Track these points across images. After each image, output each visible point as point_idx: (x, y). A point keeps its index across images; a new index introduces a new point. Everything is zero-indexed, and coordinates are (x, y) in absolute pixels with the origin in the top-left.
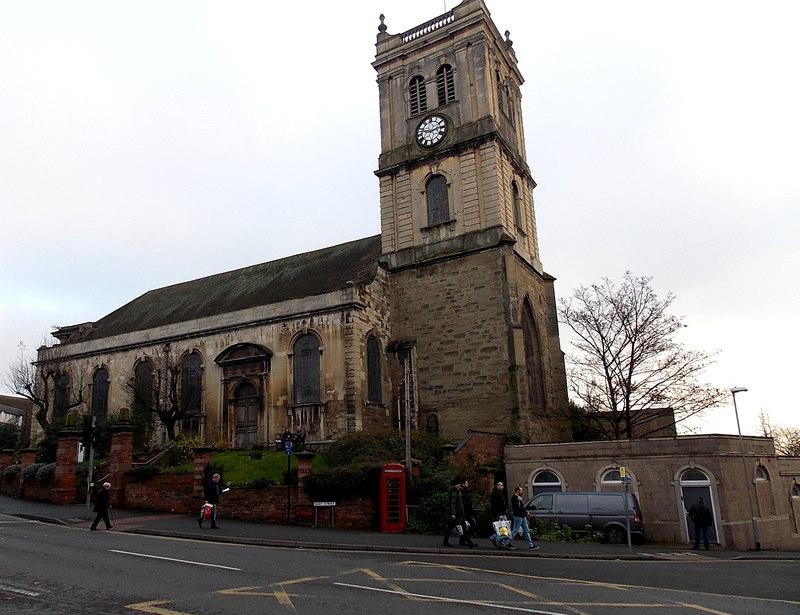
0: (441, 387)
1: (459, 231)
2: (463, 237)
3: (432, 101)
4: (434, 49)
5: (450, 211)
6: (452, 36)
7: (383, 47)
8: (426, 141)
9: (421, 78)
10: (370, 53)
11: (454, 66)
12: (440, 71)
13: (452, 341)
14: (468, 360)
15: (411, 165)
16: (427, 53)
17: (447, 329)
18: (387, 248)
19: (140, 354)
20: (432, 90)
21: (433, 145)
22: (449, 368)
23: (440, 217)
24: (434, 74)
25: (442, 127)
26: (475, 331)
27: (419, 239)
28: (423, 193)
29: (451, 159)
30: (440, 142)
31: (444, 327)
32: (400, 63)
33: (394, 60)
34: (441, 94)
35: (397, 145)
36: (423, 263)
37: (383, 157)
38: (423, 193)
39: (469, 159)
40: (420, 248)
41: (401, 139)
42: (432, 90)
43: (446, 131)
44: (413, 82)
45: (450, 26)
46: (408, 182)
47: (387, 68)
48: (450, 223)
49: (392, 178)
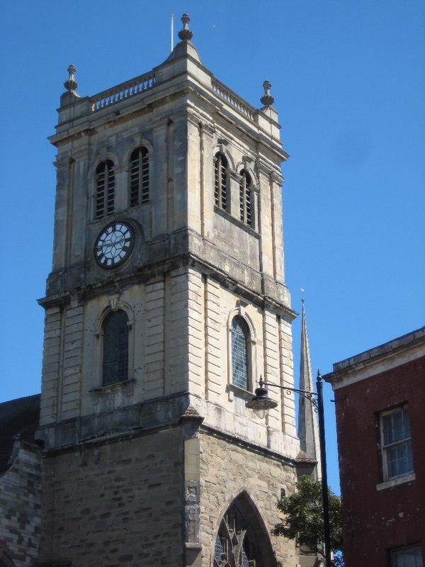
2: (141, 406)
4: (129, 123)
5: (130, 366)
6: (151, 107)
7: (67, 114)
8: (107, 259)
9: (110, 163)
10: (49, 120)
11: (150, 149)
12: (134, 156)
15: (87, 295)
16: (119, 127)
17: (113, 546)
18: (46, 417)
19: (279, 404)
20: (122, 180)
21: (115, 266)
23: (117, 369)
24: (126, 157)
26: (145, 551)
27: (91, 407)
28: (98, 336)
29: (136, 288)
30: (123, 261)
31: (107, 543)
32: (85, 139)
34: (134, 188)
35: (73, 261)
36: (83, 440)
37: (54, 279)
38: (98, 336)
39: (157, 289)
41: (78, 253)
42: (122, 180)
43: (132, 246)
44: (100, 168)
45: (143, 95)
46: (80, 319)
47: (67, 147)
49: (61, 312)
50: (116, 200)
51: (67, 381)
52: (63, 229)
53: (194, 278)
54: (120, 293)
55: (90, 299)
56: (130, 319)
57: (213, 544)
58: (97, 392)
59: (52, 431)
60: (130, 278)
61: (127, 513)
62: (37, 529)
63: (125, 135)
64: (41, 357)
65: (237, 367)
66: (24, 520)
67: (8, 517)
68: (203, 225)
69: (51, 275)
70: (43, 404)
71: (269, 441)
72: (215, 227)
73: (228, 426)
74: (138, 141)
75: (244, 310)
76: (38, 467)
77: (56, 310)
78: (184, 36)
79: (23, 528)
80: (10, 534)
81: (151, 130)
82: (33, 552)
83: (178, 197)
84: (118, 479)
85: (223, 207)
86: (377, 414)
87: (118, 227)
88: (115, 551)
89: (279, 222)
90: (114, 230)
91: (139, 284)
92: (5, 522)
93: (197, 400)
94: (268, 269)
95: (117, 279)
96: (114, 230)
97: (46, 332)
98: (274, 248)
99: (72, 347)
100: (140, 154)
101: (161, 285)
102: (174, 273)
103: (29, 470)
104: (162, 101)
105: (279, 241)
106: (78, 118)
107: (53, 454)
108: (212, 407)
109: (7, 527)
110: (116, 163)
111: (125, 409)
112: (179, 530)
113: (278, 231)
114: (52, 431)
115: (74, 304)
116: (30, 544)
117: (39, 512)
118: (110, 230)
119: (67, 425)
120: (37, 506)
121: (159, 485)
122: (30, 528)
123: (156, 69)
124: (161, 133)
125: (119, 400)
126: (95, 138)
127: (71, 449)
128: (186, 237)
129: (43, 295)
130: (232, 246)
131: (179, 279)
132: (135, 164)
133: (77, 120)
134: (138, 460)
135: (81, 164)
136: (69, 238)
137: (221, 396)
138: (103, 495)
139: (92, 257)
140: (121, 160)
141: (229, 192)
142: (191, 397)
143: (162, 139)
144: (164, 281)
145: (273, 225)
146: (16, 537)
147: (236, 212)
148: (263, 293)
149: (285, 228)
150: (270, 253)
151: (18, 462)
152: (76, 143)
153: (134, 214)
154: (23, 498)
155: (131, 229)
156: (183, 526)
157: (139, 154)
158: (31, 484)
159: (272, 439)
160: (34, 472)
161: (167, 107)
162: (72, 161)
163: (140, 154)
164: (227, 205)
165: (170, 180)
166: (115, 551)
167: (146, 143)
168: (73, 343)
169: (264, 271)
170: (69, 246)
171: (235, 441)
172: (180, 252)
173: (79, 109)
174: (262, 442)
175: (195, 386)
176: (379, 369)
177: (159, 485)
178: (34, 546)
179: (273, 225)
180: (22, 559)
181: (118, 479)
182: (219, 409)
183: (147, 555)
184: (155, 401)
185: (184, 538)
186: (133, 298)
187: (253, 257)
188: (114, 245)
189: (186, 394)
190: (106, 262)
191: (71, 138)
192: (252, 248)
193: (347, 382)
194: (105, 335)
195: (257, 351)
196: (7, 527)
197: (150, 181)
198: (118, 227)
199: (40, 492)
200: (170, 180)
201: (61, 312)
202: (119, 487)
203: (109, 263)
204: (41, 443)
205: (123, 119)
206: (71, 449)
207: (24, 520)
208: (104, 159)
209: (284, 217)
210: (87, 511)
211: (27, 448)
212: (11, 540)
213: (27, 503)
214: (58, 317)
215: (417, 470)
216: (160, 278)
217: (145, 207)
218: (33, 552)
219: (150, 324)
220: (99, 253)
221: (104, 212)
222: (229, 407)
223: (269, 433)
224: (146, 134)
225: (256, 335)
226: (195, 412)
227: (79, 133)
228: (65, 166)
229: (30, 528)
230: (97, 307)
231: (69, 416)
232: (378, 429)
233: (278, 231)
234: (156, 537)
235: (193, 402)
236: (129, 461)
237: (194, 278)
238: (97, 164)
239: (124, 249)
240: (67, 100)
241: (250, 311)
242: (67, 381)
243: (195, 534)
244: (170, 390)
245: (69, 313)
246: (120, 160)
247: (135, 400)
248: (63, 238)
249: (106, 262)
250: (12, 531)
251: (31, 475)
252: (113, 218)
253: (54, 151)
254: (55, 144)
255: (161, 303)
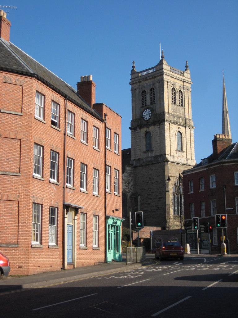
0: (147, 210)
1: (154, 154)
3: (148, 102)
4: (149, 81)
6: (155, 77)
9: (145, 92)
10: (128, 78)
12: (151, 90)
13: (150, 195)
14: (155, 201)
15: (141, 127)
16: (147, 82)
17: (150, 190)
20: (148, 97)
21: (147, 120)
22: (149, 204)
23: (149, 149)
24: (149, 91)
25: (150, 114)
26: (157, 191)
28: (144, 138)
30: (149, 119)
31: (148, 189)
32: (138, 84)
33: (136, 83)
34: (151, 99)
35: (137, 118)
37: (132, 122)
38: (144, 138)
40: (142, 159)
42: (148, 97)
43: (151, 115)
44: (143, 92)
47: (134, 85)
48: (152, 151)
49: (135, 131)
50: (147, 101)
51: (137, 149)
52: (134, 108)
53: (133, 240)
54: (149, 127)
55: (142, 128)
56: (152, 134)
57: (172, 189)
58: (145, 152)
59: (134, 161)
60: (151, 124)
61: (153, 182)
62: (132, 185)
63: (148, 84)
64: (130, 140)
65: (178, 145)
66: (129, 183)
67: (125, 183)
68: (169, 110)
69: (132, 121)
70: (131, 150)
71: (187, 162)
72: (172, 109)
73: (176, 160)
74: (152, 86)
75: (180, 130)
76: (131, 171)
77: (134, 130)
78: (162, 57)
79: (129, 185)
80: (121, 151)
81: (155, 84)
82: (132, 191)
83: (162, 103)
84: (150, 174)
85: (174, 102)
86: (189, 181)
87: (148, 110)
88: (150, 191)
89: (190, 102)
90: (147, 111)
91: (153, 125)
92: (125, 184)
93: (168, 156)
94: (187, 117)
95: (148, 124)
96: (147, 111)
97: (131, 136)
98: (189, 110)
99: (138, 140)
100: (152, 90)
101: (159, 126)
102: (162, 124)
103: (129, 172)
104: (157, 76)
105: (190, 107)
106: (136, 78)
107: (135, 167)
108: (172, 157)
109: (125, 186)
110: (147, 92)
111: (151, 157)
112: (164, 187)
113: (190, 105)
114: (134, 161)
115: (138, 129)
116: (130, 189)
117: (132, 181)
118: (146, 110)
119: (138, 160)
120: (132, 180)
121: (159, 176)
122: (130, 185)
123: (156, 66)
124: (157, 85)
125: (150, 154)
126: (141, 84)
127: (139, 166)
128: (164, 114)
129: (130, 127)
130: (177, 113)
131: (163, 125)
132: (151, 92)
133: (137, 80)
134: (155, 170)
135: (138, 91)
136: (136, 111)
137: (174, 153)
138: (147, 178)
139: (142, 117)
140: (148, 91)
141: (176, 98)
142: (166, 155)
143: (158, 87)
144: (159, 125)
145: (188, 104)
146: (127, 188)
147: (178, 103)
148: (185, 124)
149: (192, 104)
150: (188, 110)
151: (127, 170)
152: (136, 85)
153: (152, 106)
154: (128, 178)
155: (151, 111)
156: (165, 186)
157: (152, 89)
158: (130, 175)
159: (188, 161)
160: (131, 172)
161: (159, 78)
162: (135, 90)
163: (152, 90)
164: (175, 100)
165: (160, 98)
166: (150, 191)
167: (154, 87)
168: (138, 139)
169: (186, 117)
170: (136, 113)
171: (178, 163)
172: (163, 119)
173: (136, 75)
174: (185, 163)
175: (167, 152)
176: (189, 173)
177: (159, 176)
178: (131, 189)
179: (188, 104)
180: (129, 192)
181: (150, 174)
182: (174, 156)
183: (158, 192)
184: (158, 156)
185: (165, 189)
186: (152, 129)
187: (183, 114)
188: (147, 115)
189: (165, 154)
190: (145, 119)
191: (135, 83)
192: (182, 112)
193: (185, 174)
194: (146, 138)
195: (184, 139)
196: (125, 186)
197: (155, 95)
198: (148, 110)
199: (132, 176)
200: (160, 98)
201: (135, 131)
202: (150, 176)
203: (146, 119)
204: (132, 165)
205: (148, 80)
206: (139, 166)
207: (129, 183)
208: (143, 90)
209: (192, 101)
210: (143, 181)
211: (129, 166)
212: (126, 189)
213: (129, 179)
214: (134, 132)
215: (194, 191)
216: (158, 124)
217: (154, 105)
218: (132, 191)
219: (156, 136)
220: (144, 119)
221: (145, 107)
222: (177, 155)
223: (187, 160)
224: (154, 84)
225: (184, 135)
226: (167, 159)
227: (137, 82)
228: (133, 90)
229: (130, 185)
230: (144, 130)
231: (138, 158)
232: (189, 183)
233: (190, 105)
234: (159, 188)
235: (167, 156)
236: (152, 170)
237: (133, 240)
238: (141, 91)
239: (149, 116)
240: (133, 72)
241: (182, 129)
242: (137, 149)
243: (168, 188)
244: (162, 153)
245: (137, 132)
246: (148, 91)
247: (154, 155)
248: (134, 111)
249: (145, 119)
250: (126, 186)
251: (130, 173)
252: (146, 107)
253: (130, 86)
254: (131, 84)
255: (159, 131)
